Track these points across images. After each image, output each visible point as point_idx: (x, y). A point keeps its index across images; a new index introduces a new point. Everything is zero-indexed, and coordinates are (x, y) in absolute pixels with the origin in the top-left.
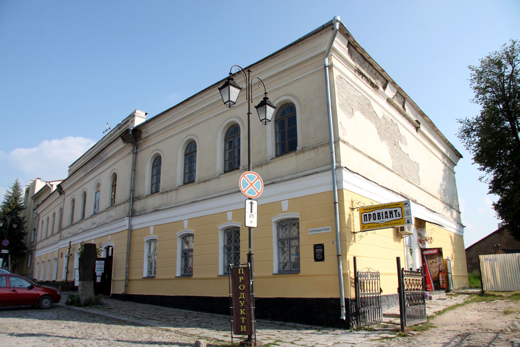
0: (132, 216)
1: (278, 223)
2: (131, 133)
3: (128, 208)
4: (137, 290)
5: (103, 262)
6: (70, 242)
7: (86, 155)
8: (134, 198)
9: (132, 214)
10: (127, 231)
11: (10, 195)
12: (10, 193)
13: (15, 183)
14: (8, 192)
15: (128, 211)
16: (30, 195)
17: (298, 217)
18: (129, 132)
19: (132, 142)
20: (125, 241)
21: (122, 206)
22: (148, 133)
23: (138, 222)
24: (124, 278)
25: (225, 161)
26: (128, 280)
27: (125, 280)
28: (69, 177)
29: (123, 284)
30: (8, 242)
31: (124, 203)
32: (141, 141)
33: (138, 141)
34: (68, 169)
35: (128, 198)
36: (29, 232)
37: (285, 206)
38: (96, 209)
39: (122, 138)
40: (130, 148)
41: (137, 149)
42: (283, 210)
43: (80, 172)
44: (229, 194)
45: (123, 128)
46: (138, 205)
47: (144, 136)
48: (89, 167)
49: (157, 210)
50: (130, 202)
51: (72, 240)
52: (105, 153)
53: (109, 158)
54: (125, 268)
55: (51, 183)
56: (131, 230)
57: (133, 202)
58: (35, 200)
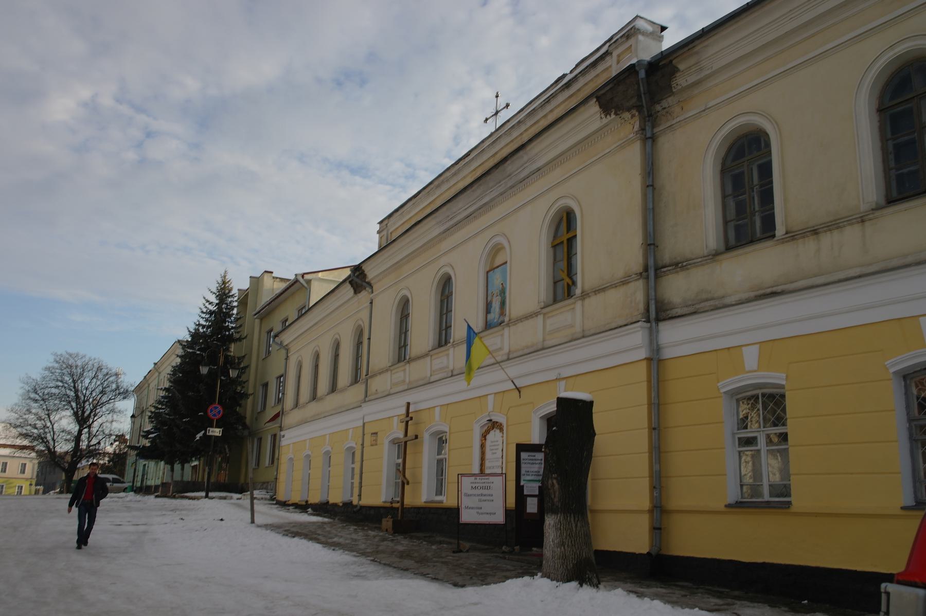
0: (658, 320)
1: (905, 377)
2: (642, 74)
3: (640, 297)
4: (693, 541)
5: (540, 456)
6: (409, 404)
7: (436, 183)
8: (655, 268)
9: (658, 311)
10: (644, 364)
11: (212, 308)
12: (211, 303)
13: (220, 280)
14: (208, 301)
15: (641, 307)
16: (250, 312)
17: (784, 383)
18: (637, 73)
19: (639, 108)
20: (640, 393)
21: (614, 297)
22: (701, 69)
23: (677, 337)
24: (646, 504)
25: (726, 222)
26: (660, 512)
27: (651, 511)
28: (381, 249)
29: (644, 523)
30: (220, 408)
31: (624, 282)
32: (671, 100)
33: (658, 102)
34: (377, 227)
35: (640, 269)
36: (251, 391)
37: (750, 357)
38: (494, 316)
39: (598, 99)
40: (627, 126)
41: (653, 127)
42: (747, 369)
43: (430, 222)
44: (860, 277)
45: (613, 67)
46: (677, 288)
47: (681, 81)
48: (462, 207)
49: (774, 294)
50: (647, 278)
51: (411, 397)
52: (525, 158)
53: (539, 169)
54: (646, 473)
55: (306, 277)
56: (660, 361)
57: (657, 277)
58: (261, 320)
